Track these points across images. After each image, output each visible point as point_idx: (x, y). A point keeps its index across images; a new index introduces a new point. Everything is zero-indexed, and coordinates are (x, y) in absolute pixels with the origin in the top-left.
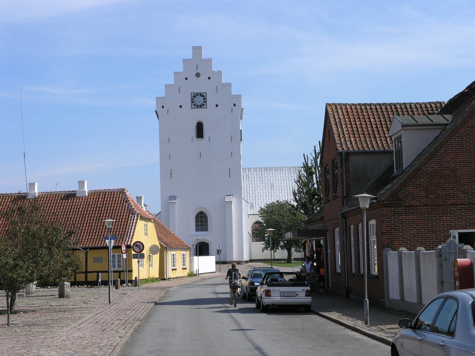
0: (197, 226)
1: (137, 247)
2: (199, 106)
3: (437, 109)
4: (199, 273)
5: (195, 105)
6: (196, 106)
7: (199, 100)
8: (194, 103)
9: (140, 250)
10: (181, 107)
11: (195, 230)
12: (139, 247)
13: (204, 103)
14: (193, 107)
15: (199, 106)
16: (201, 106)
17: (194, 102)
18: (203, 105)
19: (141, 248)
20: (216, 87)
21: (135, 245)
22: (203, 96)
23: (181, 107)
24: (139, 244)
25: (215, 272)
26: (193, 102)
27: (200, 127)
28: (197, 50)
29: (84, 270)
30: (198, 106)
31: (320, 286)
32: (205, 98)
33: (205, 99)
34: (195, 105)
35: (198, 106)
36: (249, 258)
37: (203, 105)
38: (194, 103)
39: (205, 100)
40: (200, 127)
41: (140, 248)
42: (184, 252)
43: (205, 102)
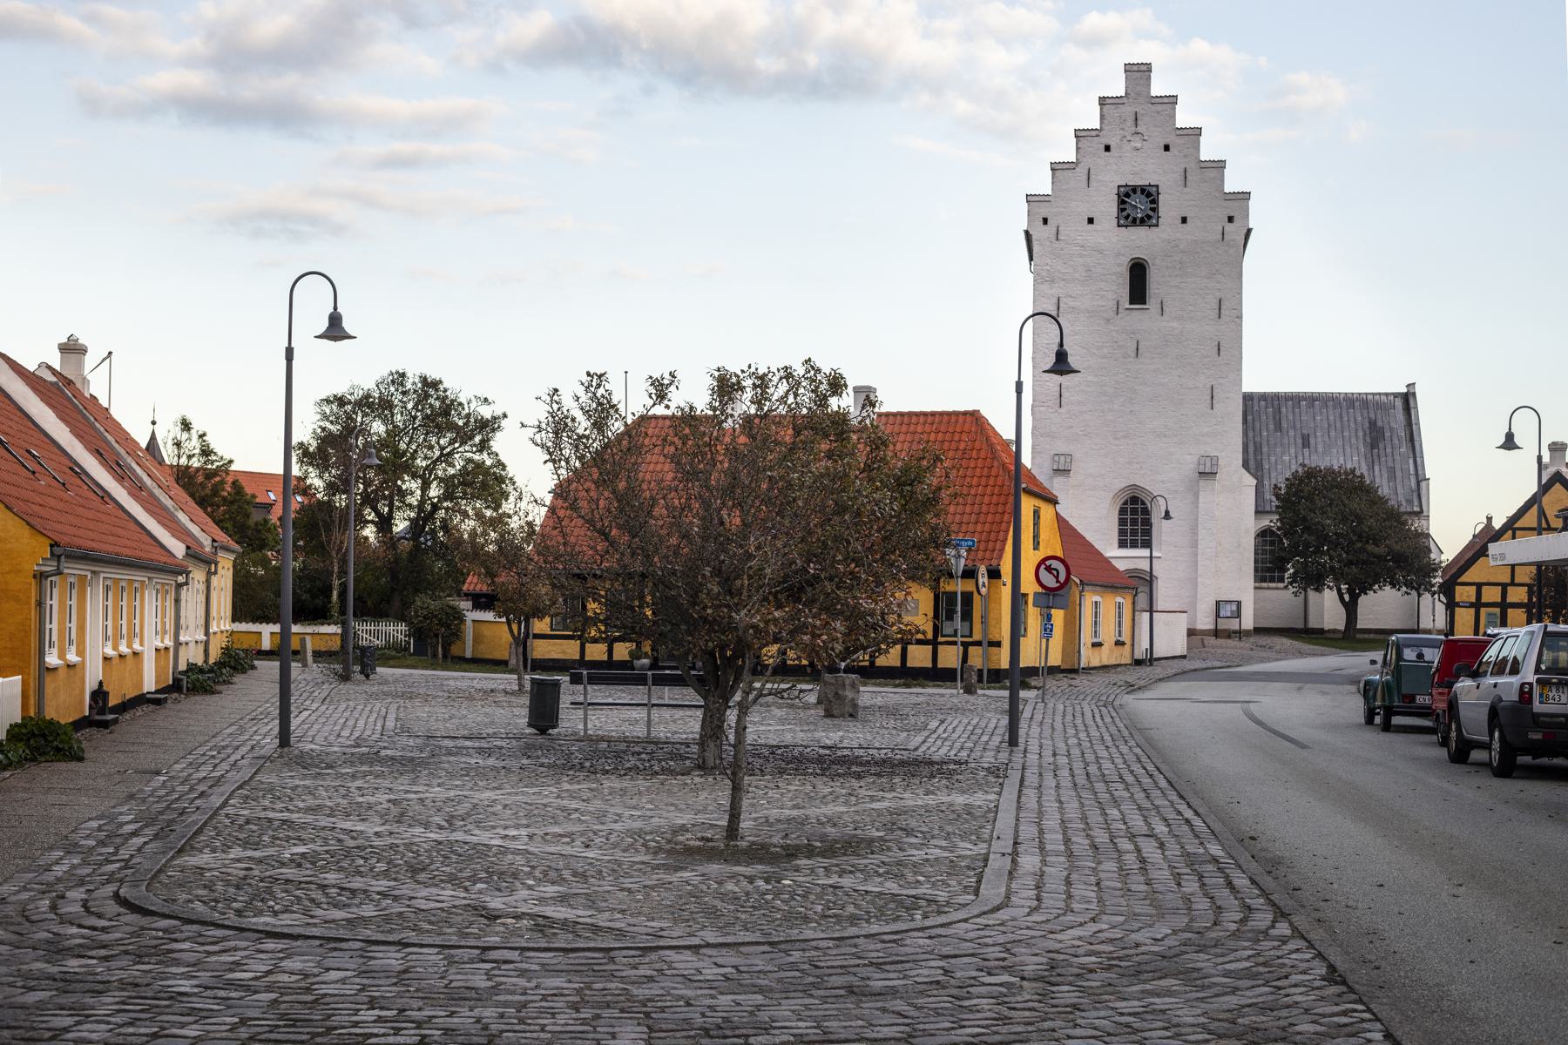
0: (1122, 532)
1: (1051, 573)
2: (1138, 221)
3: (345, 582)
4: (1155, 656)
5: (1127, 217)
6: (1130, 219)
7: (1139, 204)
8: (1125, 213)
9: (1058, 581)
10: (1091, 221)
11: (1117, 545)
12: (1055, 572)
13: (1151, 213)
14: (1122, 222)
15: (1138, 221)
16: (1144, 221)
17: (1125, 209)
18: (1149, 217)
19: (1062, 578)
20: (1183, 170)
21: (1043, 566)
22: (1149, 195)
23: (1091, 221)
24: (1055, 564)
25: (1184, 657)
26: (1123, 210)
27: (1138, 273)
28: (1138, 73)
29: (1483, 611)
30: (1134, 220)
31: (516, 677)
32: (1154, 200)
33: (1153, 202)
34: (1127, 217)
35: (1134, 220)
36: (1254, 623)
37: (1149, 217)
38: (1125, 213)
39: (1122, 206)
40: (1138, 273)
41: (1057, 577)
42: (1119, 599)
43: (1153, 210)
